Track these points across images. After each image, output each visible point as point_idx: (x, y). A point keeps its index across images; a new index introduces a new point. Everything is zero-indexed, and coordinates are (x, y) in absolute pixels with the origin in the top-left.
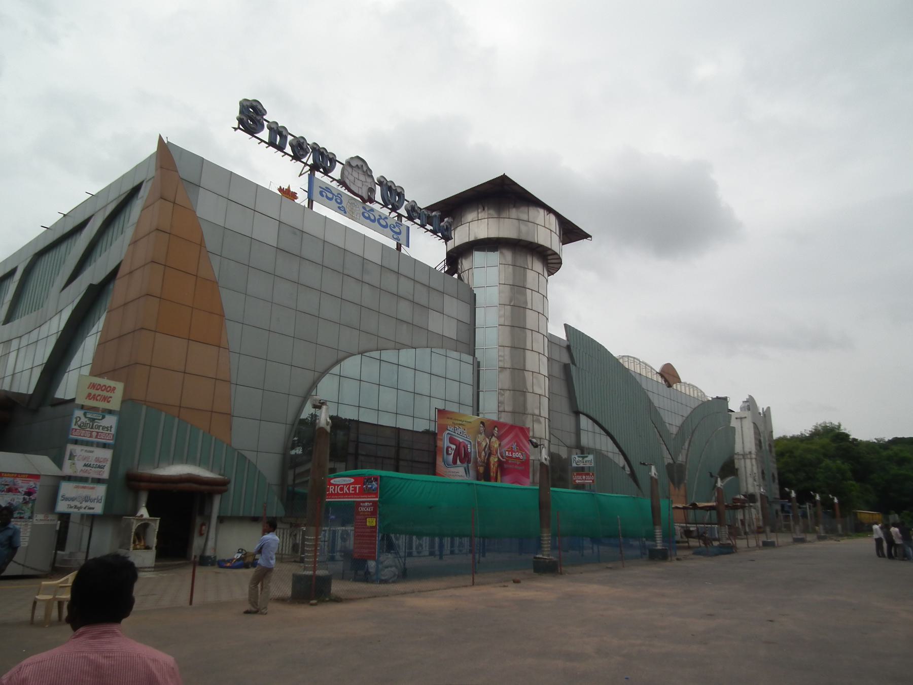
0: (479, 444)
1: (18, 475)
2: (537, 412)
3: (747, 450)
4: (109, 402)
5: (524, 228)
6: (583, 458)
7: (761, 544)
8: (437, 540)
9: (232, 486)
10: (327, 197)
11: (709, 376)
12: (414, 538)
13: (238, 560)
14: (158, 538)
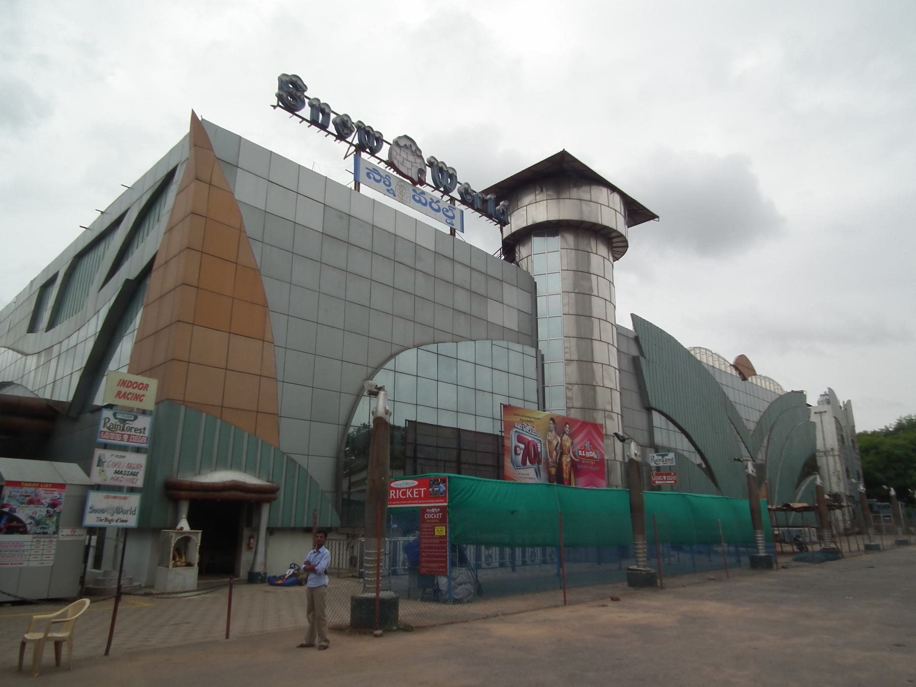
0: (550, 442)
1: (40, 485)
2: (608, 408)
3: (829, 447)
4: (141, 401)
5: (585, 207)
6: (663, 456)
7: (862, 547)
8: (518, 551)
9: (281, 493)
10: (374, 179)
11: (785, 371)
12: (483, 548)
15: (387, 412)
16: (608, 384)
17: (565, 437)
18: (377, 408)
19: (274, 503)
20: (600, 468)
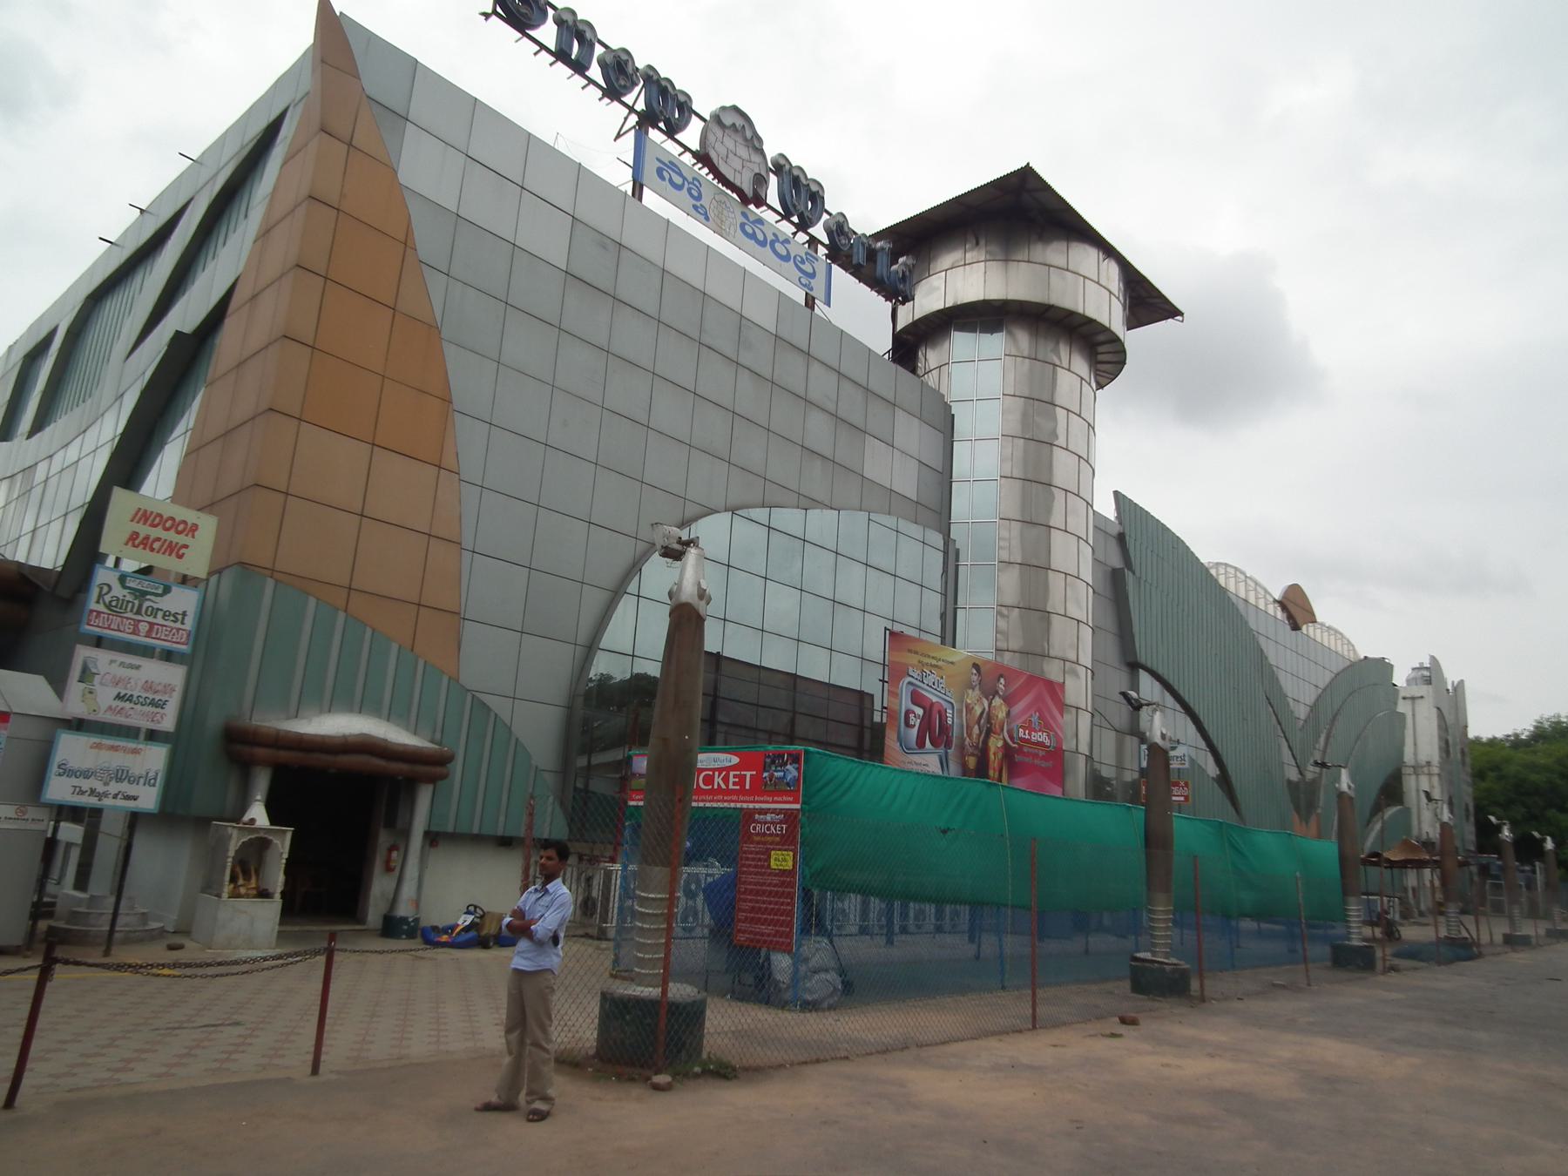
0: (969, 709)
3: (1423, 758)
7: (1498, 938)
8: (897, 904)
9: (457, 768)
10: (671, 181)
13: (467, 929)
14: (286, 873)
15: (702, 594)
16: (1074, 611)
17: (997, 701)
18: (679, 584)
19: (440, 784)
20: (1055, 762)
